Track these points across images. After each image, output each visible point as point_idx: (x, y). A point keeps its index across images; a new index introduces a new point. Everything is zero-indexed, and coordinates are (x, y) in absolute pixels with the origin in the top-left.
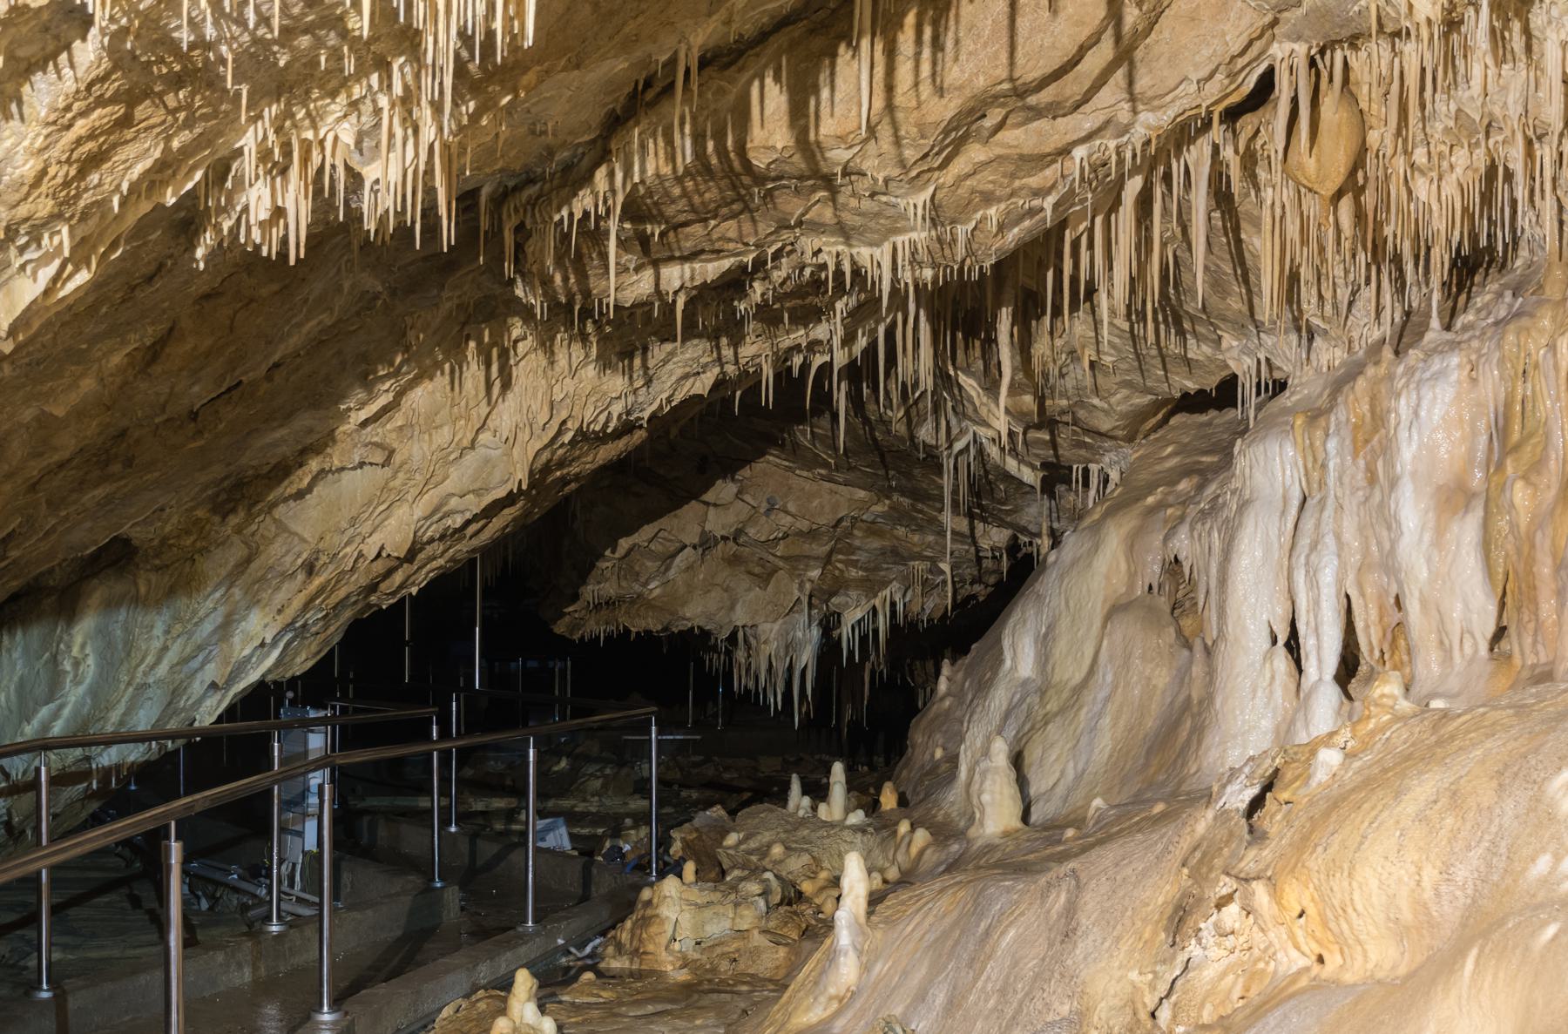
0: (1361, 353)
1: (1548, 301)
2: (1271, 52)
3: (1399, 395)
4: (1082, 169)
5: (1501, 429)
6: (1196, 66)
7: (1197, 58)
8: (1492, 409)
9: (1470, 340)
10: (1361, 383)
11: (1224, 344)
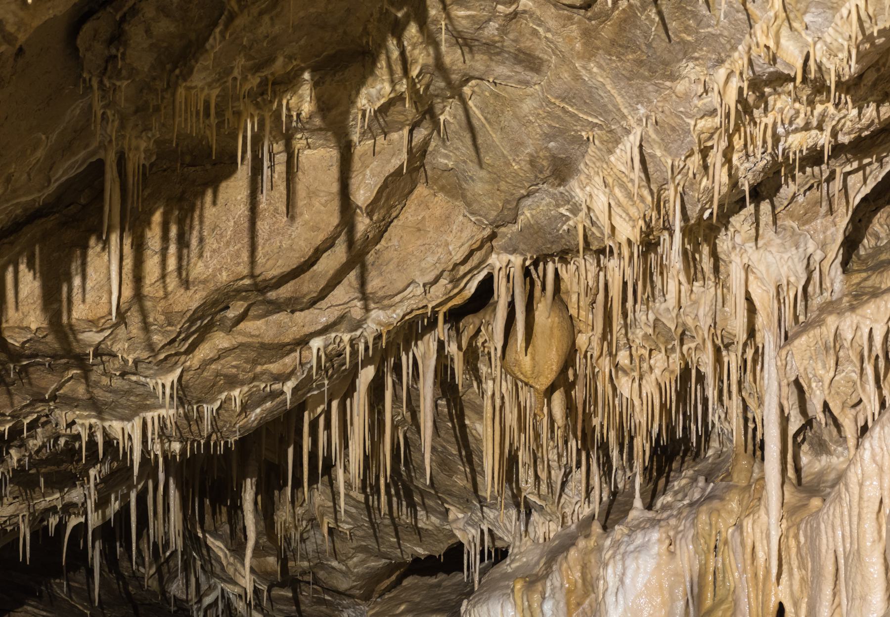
1: (736, 486)
2: (490, 261)
3: (606, 565)
4: (319, 358)
6: (423, 271)
7: (423, 265)
8: (688, 579)
10: (573, 553)
11: (451, 516)
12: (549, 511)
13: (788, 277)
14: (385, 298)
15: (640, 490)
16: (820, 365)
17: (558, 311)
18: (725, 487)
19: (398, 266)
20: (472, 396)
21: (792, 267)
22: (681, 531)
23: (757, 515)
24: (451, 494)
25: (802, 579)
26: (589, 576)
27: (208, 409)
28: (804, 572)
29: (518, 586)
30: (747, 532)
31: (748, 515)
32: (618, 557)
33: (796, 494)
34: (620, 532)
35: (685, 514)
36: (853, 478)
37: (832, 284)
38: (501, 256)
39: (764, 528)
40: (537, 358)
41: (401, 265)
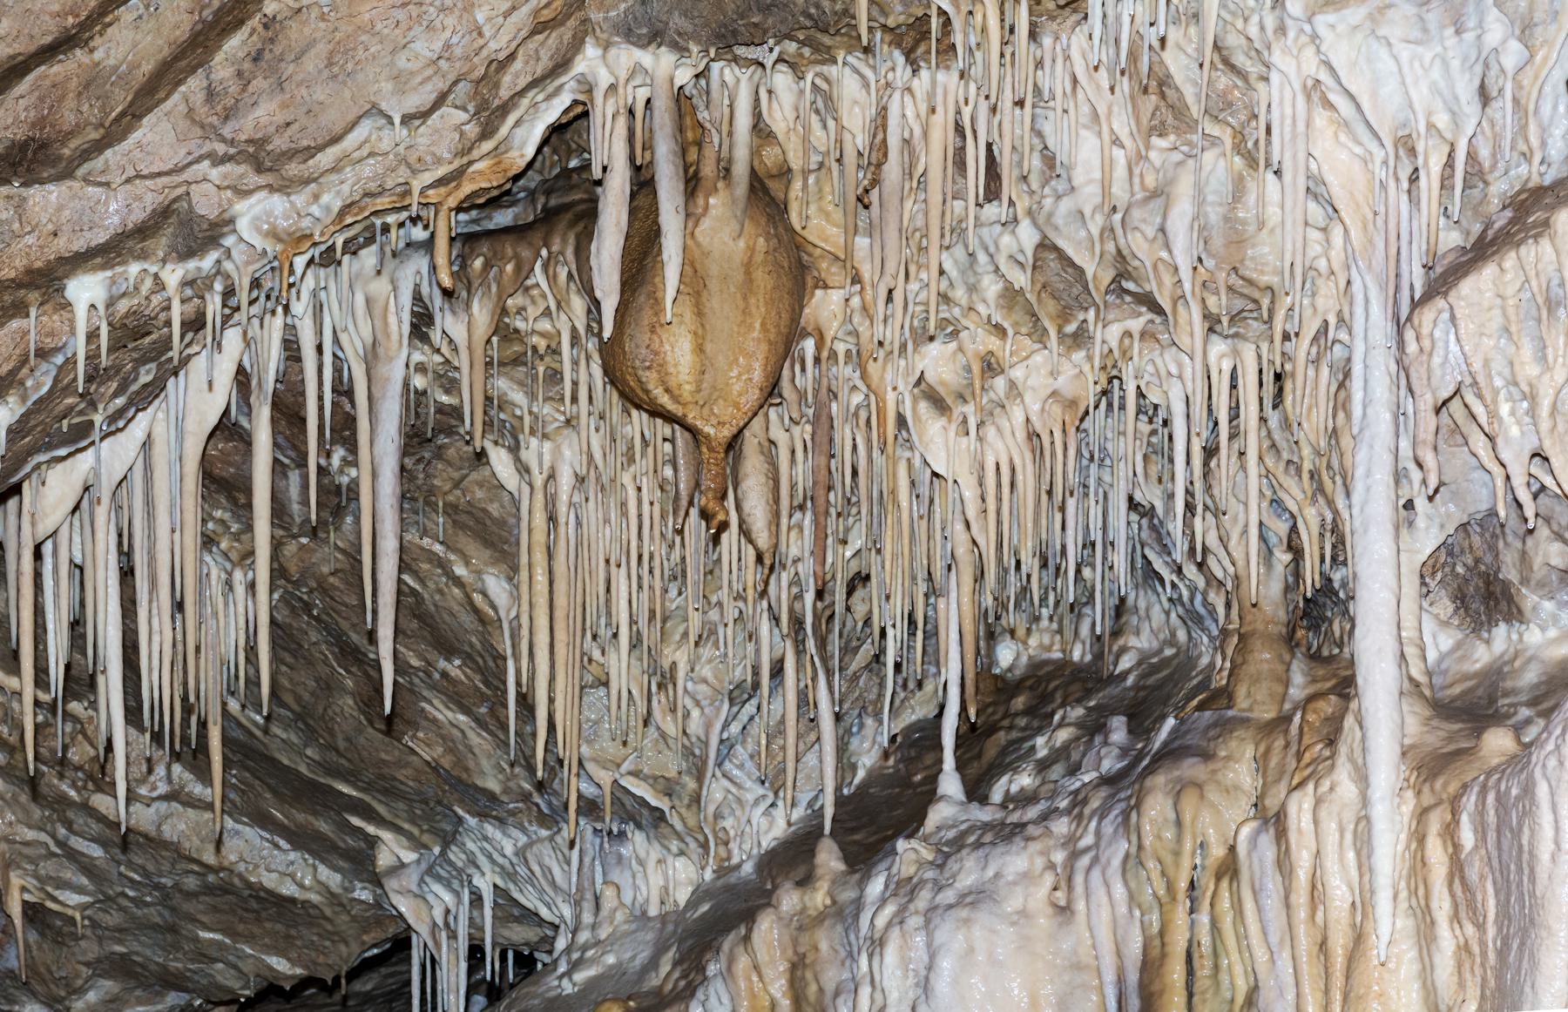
0: (748, 868)
1: (1244, 722)
2: (580, 66)
3: (877, 944)
4: (92, 336)
6: (401, 81)
7: (402, 62)
8: (1110, 977)
9: (1045, 817)
10: (767, 929)
11: (384, 860)
12: (679, 826)
13: (1429, 114)
14: (290, 155)
15: (957, 747)
16: (1527, 351)
17: (763, 221)
18: (1215, 725)
19: (330, 64)
20: (479, 494)
21: (1442, 84)
22: (1087, 850)
23: (1325, 785)
24: (391, 791)
25: (1465, 948)
26: (812, 989)
28: (1470, 930)
30: (1299, 830)
31: (1301, 784)
32: (914, 921)
33: (1435, 723)
34: (913, 856)
35: (1095, 803)
37: (1544, 144)
38: (613, 51)
39: (1349, 817)
40: (708, 347)
41: (338, 63)
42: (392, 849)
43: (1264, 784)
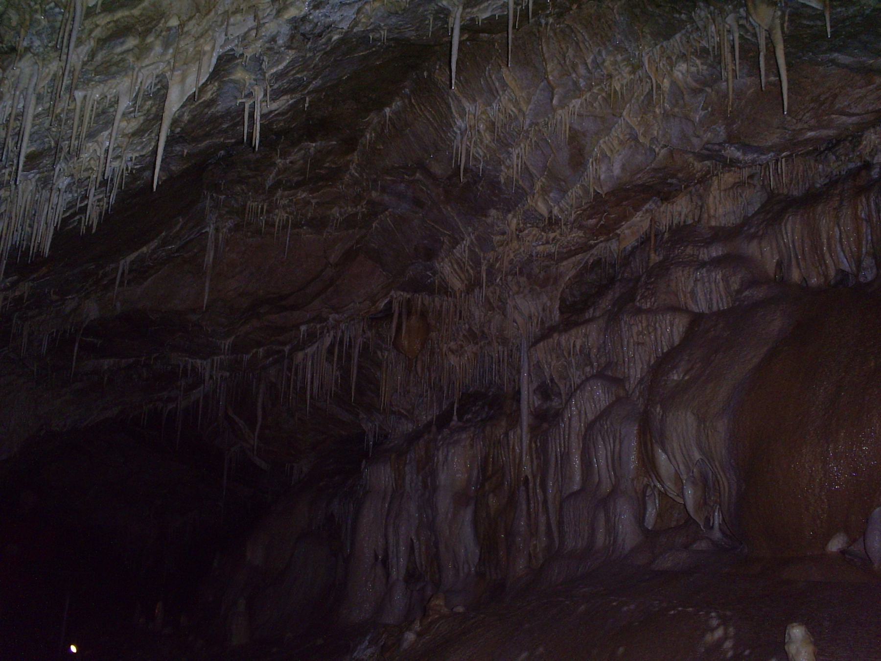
3: (438, 450)
5: (483, 468)
10: (421, 442)
11: (361, 417)
27: (247, 357)
29: (393, 456)
36: (567, 415)
42: (362, 415)
43: (720, 235)
